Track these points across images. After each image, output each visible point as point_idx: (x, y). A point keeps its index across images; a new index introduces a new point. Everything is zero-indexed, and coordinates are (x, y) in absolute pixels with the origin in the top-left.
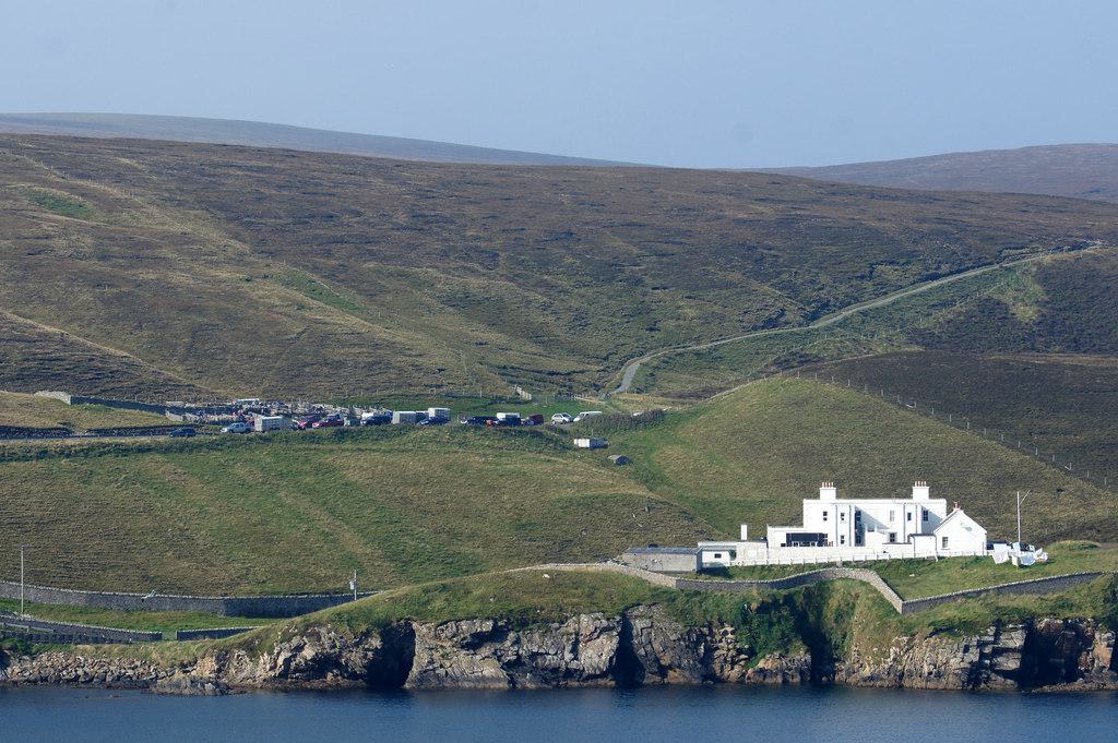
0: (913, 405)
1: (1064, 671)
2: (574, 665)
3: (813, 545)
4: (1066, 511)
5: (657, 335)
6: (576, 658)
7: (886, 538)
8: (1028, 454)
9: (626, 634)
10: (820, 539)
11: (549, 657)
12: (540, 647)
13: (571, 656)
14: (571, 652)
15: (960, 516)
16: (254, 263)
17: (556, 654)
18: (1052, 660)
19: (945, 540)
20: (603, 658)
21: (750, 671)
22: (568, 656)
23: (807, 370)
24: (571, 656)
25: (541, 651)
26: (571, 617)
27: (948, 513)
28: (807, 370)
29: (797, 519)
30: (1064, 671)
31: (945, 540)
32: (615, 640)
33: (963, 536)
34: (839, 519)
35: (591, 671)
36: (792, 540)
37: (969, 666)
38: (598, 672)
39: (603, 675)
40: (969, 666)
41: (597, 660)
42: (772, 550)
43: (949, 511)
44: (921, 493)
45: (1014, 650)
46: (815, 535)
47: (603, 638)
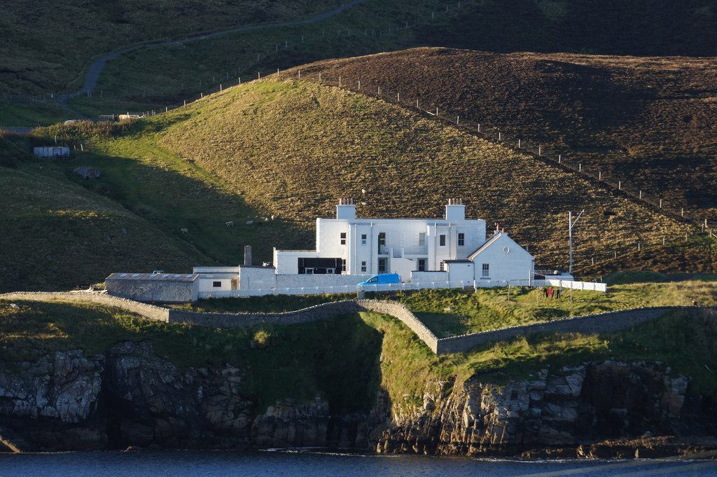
0: (435, 112)
1: (627, 423)
2: (48, 411)
3: (330, 272)
4: (614, 236)
5: (127, 28)
6: (51, 403)
7: (414, 265)
8: (571, 171)
9: (109, 376)
10: (336, 265)
11: (19, 402)
12: (7, 390)
13: (45, 401)
14: (45, 396)
15: (500, 236)
16: (451, 400)
17: (26, 399)
18: (613, 409)
19: (486, 267)
20: (83, 403)
21: (256, 421)
22: (41, 401)
23: (308, 71)
24: (45, 401)
25: (9, 395)
26: (45, 355)
27: (487, 237)
28: (308, 71)
29: (308, 241)
30: (627, 423)
31: (486, 267)
32: (96, 384)
33: (507, 260)
34: (367, 265)
35: (68, 419)
36: (306, 266)
37: (516, 415)
38: (76, 420)
39: (83, 423)
40: (516, 415)
41: (75, 406)
42: (282, 272)
43: (490, 230)
44: (455, 211)
45: (570, 398)
46: (333, 260)
47: (81, 382)
